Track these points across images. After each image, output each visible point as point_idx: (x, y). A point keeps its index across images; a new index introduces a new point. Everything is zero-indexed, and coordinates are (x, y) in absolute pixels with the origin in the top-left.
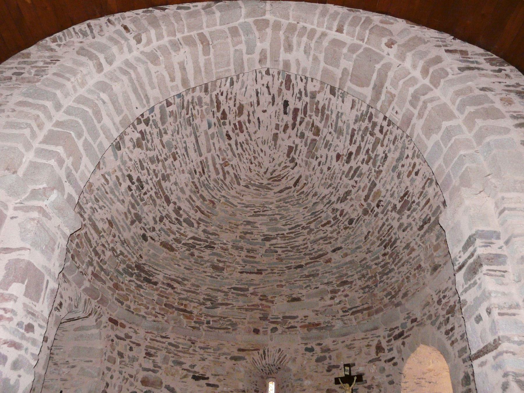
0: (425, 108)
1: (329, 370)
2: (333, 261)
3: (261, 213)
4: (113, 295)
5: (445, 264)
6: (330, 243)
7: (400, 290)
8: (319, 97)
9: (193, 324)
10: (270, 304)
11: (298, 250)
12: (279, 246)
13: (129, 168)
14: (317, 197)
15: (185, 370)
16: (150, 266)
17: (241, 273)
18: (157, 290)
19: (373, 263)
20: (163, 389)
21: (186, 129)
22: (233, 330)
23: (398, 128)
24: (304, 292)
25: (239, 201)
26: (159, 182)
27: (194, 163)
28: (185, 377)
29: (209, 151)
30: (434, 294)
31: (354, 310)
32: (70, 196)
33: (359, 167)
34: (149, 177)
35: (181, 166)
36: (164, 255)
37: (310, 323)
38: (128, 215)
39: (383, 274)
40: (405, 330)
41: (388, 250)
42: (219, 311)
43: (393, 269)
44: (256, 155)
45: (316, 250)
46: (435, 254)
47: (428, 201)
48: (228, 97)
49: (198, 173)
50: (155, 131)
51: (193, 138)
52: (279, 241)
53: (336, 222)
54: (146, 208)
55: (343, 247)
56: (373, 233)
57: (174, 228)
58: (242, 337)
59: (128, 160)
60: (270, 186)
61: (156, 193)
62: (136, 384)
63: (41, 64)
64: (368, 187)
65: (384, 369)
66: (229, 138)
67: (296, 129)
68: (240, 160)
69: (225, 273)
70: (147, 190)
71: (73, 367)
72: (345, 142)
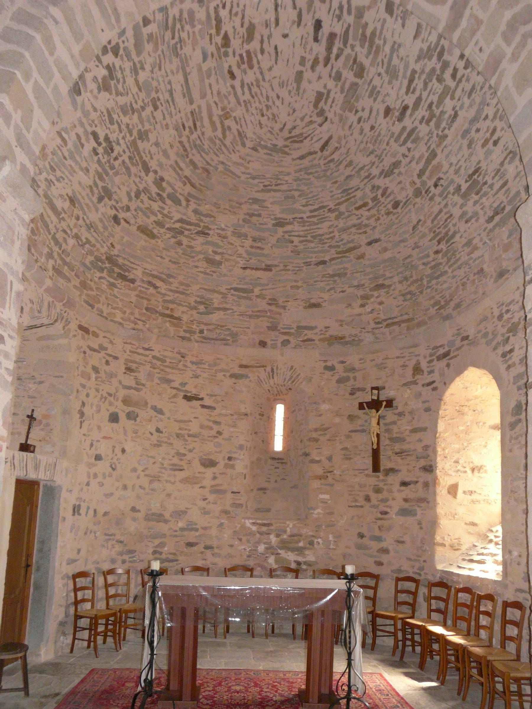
0: (524, 46)
2: (367, 257)
3: (274, 187)
4: (80, 296)
5: (515, 270)
6: (365, 232)
7: (451, 300)
8: (369, 17)
9: (182, 334)
10: (281, 311)
11: (321, 240)
12: (296, 234)
13: (93, 121)
14: (351, 168)
15: (174, 388)
16: (124, 258)
17: (244, 268)
18: (135, 289)
19: (421, 262)
20: (149, 410)
21: (171, 63)
22: (233, 342)
23: (479, 73)
24: (326, 296)
25: (243, 170)
26: (134, 143)
27: (183, 114)
28: (175, 396)
29: (203, 96)
30: (495, 307)
31: (390, 321)
32: (23, 169)
33: (416, 128)
34: (121, 135)
35: (164, 118)
36: (143, 243)
37: (331, 336)
38: (95, 189)
39: (432, 277)
40: (452, 349)
41: (443, 246)
42: (215, 317)
43: (446, 272)
44: (270, 103)
45: (345, 241)
46: (503, 256)
47: (505, 184)
48: (234, 11)
49: (187, 129)
50: (128, 65)
51: (180, 77)
52: (296, 227)
53: (376, 205)
54: (117, 180)
55: (383, 238)
56: (425, 222)
57: (155, 206)
58: (246, 353)
59: (91, 110)
60: (286, 150)
61: (130, 158)
62: (116, 404)
64: (425, 158)
65: (420, 394)
66: (233, 76)
67: (329, 66)
68: (247, 110)
69: (223, 269)
70: (119, 154)
71: (41, 383)
72: (400, 88)
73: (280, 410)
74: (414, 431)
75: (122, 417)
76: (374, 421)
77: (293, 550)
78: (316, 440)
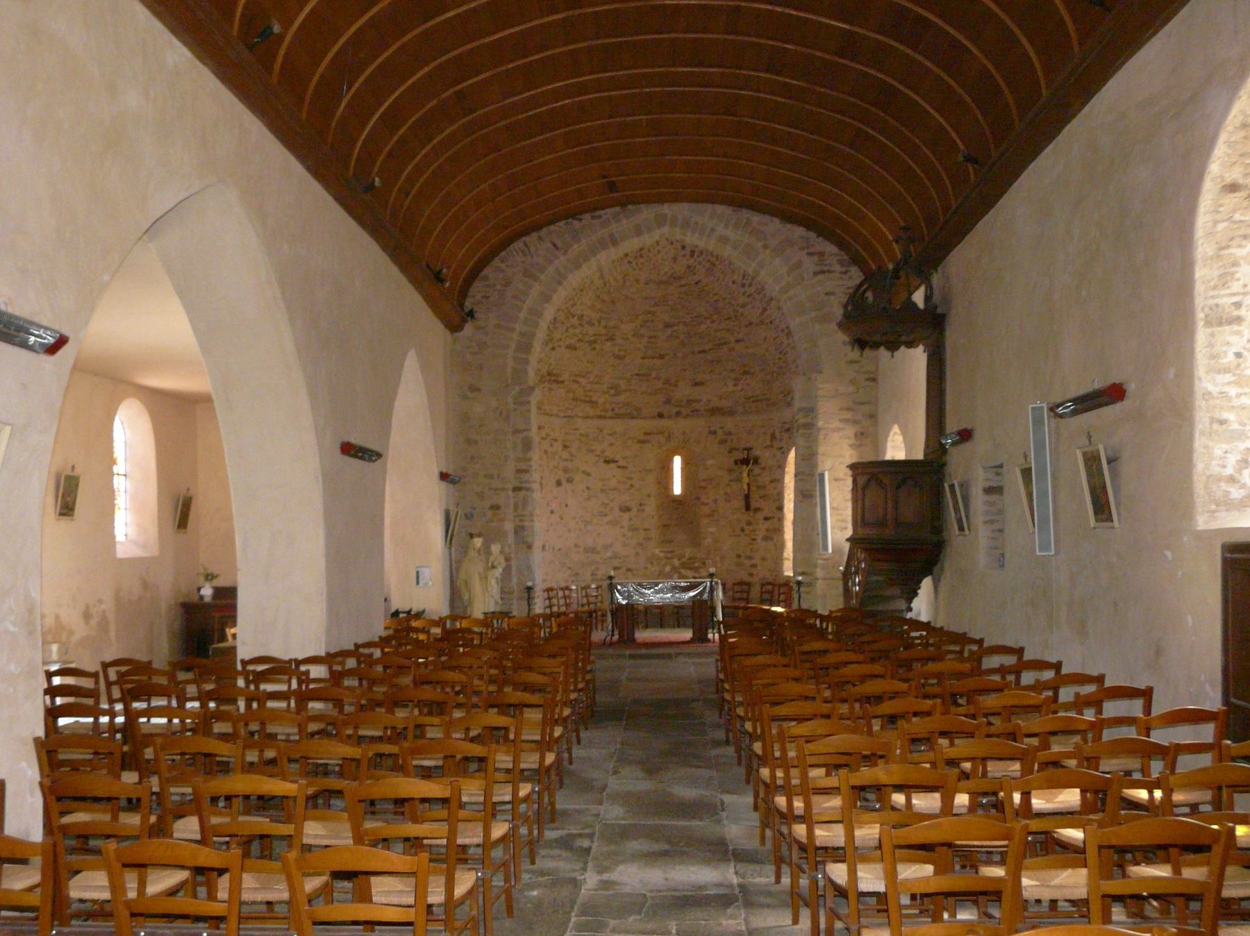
1: (730, 452)
42: (622, 398)
52: (681, 327)
69: (627, 360)
73: (677, 462)
74: (772, 481)
75: (564, 481)
76: (745, 475)
77: (690, 569)
78: (704, 488)
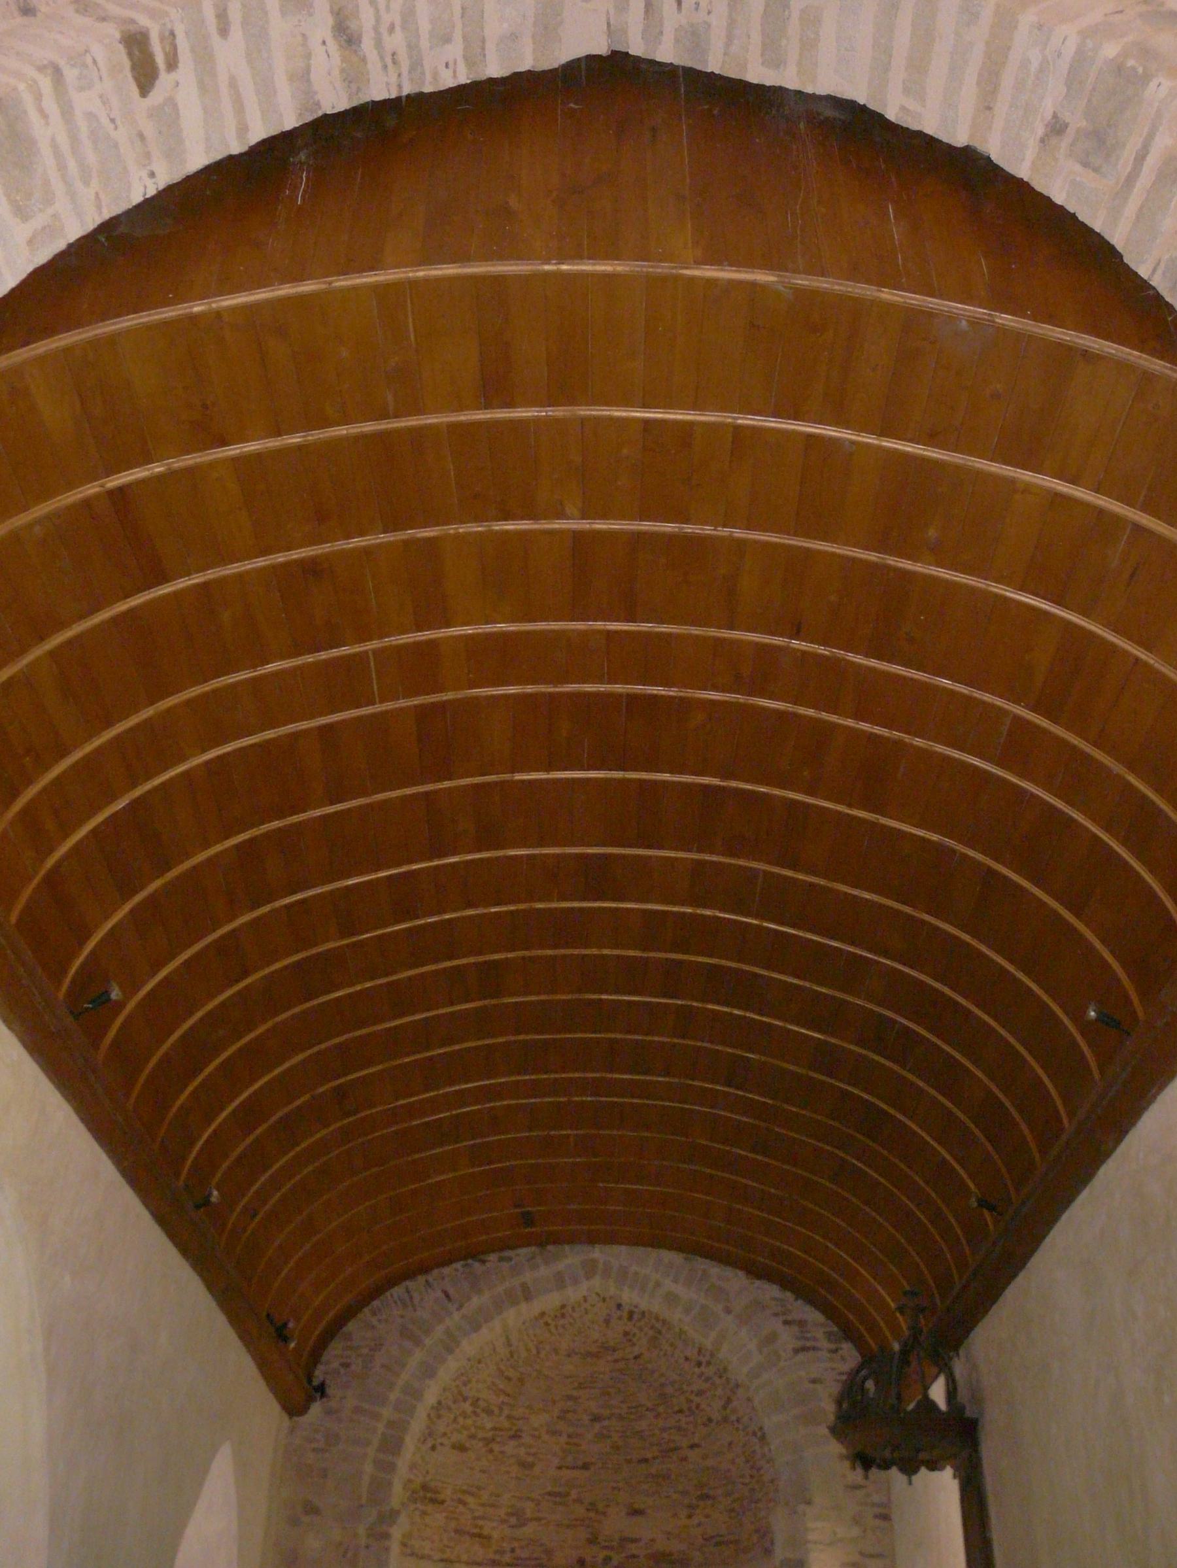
31: (718, 1539)
42: (528, 1530)
63: (365, 1351)
